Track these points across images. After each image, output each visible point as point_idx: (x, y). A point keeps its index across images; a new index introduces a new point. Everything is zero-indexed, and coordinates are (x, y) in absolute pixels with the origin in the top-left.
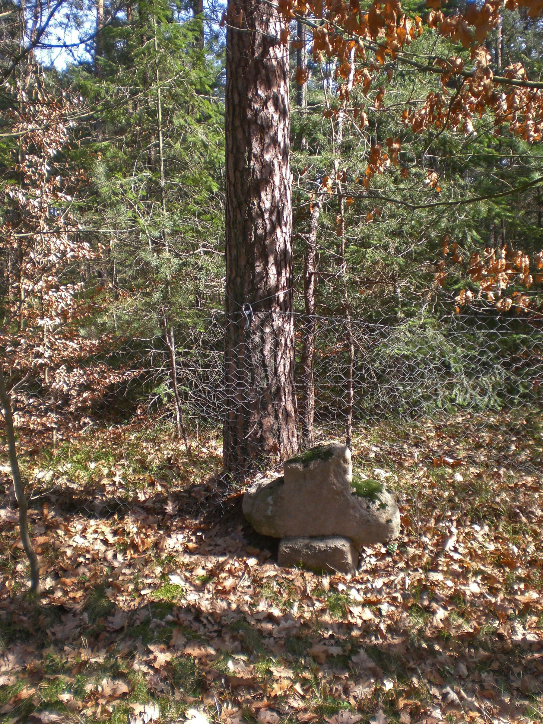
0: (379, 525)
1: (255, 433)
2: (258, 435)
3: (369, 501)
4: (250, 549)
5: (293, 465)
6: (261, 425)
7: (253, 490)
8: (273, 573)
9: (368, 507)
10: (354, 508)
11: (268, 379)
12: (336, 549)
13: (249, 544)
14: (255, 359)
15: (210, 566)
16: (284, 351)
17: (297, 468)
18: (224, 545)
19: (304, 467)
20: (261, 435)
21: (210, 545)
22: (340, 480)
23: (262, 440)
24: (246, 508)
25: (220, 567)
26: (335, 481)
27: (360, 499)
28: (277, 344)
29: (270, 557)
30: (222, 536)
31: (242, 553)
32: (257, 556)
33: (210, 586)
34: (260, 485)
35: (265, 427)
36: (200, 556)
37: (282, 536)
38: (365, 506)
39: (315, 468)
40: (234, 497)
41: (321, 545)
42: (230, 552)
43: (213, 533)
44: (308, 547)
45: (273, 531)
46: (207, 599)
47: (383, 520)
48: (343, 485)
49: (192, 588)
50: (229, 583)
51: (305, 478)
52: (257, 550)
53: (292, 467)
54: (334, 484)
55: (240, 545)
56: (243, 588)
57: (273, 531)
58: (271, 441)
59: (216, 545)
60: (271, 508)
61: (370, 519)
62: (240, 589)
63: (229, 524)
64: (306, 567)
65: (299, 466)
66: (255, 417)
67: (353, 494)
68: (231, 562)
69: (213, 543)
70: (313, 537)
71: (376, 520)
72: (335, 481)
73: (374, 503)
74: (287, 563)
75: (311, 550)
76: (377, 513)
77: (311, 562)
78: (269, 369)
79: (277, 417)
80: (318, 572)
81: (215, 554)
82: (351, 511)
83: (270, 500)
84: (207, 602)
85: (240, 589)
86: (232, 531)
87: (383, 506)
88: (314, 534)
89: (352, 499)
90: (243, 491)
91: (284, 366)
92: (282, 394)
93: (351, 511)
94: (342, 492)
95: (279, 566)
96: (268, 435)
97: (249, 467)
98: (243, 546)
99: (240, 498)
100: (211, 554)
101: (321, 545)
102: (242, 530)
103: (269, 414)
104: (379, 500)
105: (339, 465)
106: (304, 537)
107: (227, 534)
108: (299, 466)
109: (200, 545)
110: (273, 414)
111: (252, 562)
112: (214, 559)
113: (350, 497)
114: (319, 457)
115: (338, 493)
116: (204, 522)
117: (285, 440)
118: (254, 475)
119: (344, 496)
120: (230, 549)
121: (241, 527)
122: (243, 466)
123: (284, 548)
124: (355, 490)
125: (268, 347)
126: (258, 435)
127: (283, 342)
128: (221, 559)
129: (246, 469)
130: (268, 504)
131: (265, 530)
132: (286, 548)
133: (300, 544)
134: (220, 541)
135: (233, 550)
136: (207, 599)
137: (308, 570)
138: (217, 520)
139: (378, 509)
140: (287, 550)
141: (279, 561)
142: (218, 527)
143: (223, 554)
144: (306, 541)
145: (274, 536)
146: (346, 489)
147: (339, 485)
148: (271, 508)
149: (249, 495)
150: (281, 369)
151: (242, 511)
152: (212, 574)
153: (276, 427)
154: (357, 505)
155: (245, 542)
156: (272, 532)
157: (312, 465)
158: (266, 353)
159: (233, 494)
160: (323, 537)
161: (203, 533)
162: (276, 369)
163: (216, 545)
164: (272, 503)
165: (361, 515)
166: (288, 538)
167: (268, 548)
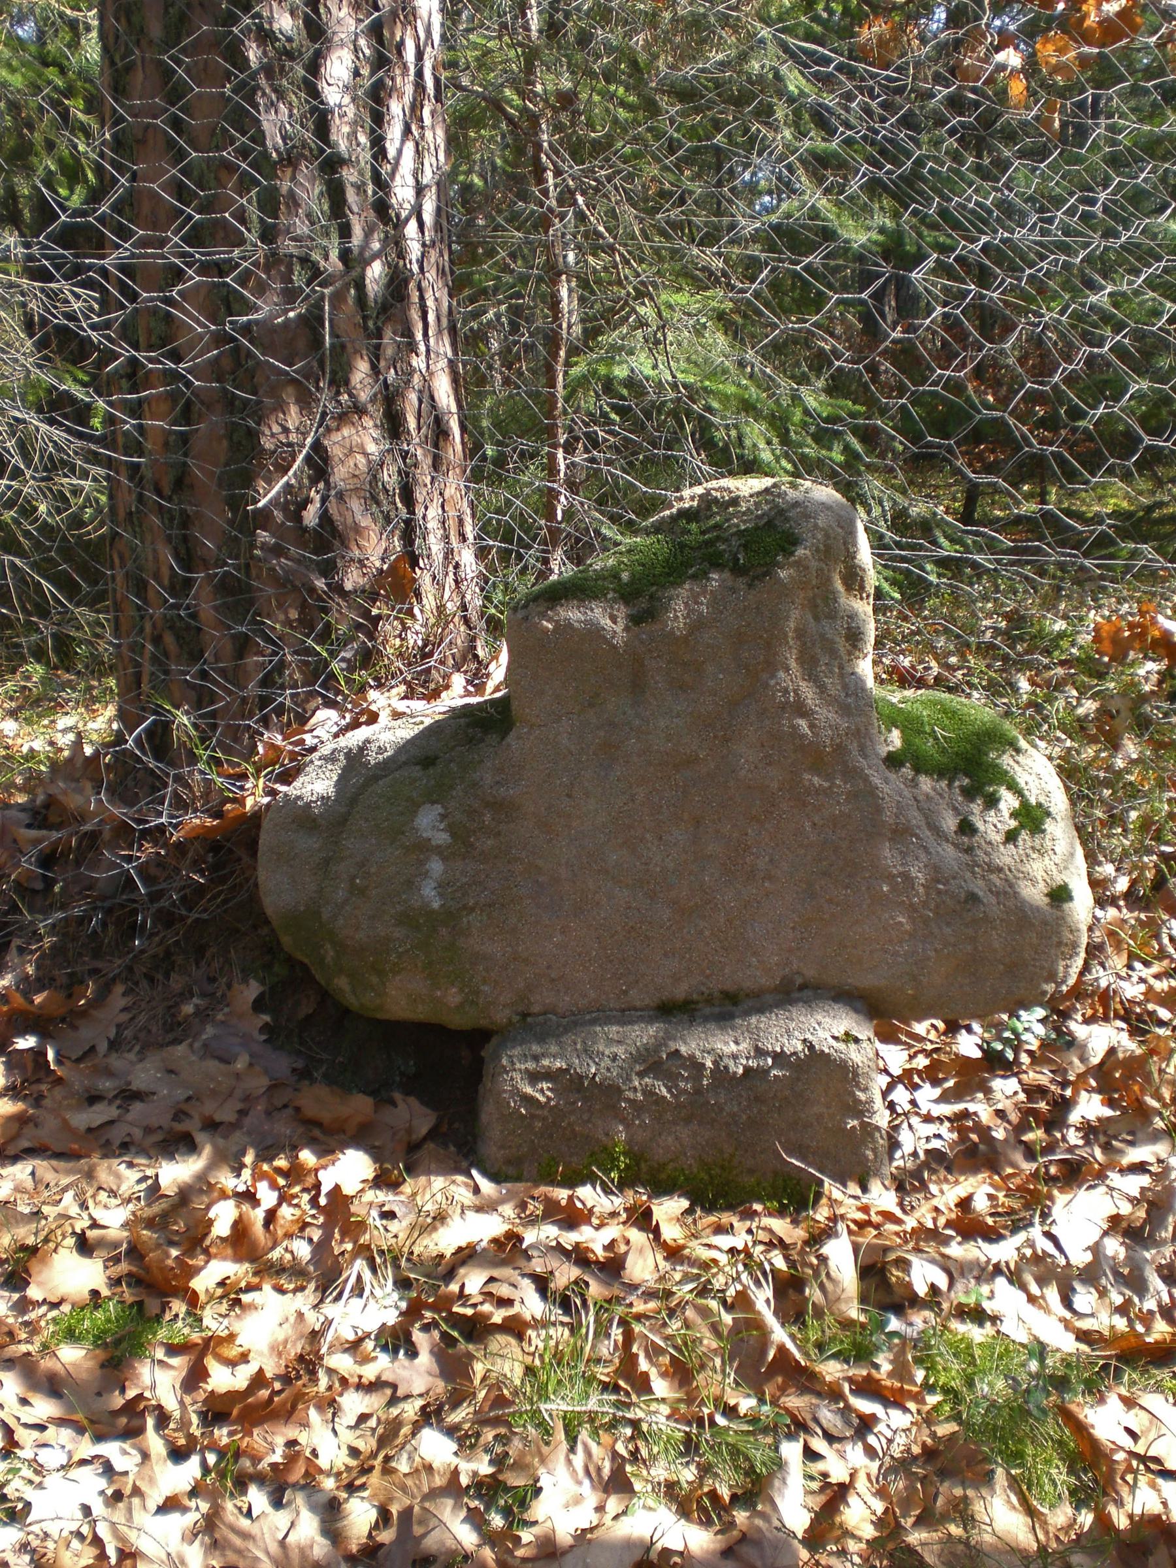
0: (1021, 917)
1: (295, 504)
2: (311, 516)
3: (970, 794)
4: (318, 1100)
5: (573, 614)
6: (320, 465)
7: (317, 785)
8: (484, 1229)
9: (967, 828)
10: (901, 834)
11: (345, 232)
12: (815, 1061)
13: (304, 1074)
14: (277, 123)
15: (114, 1219)
16: (416, 107)
17: (594, 632)
18: (168, 1093)
19: (636, 620)
20: (325, 517)
21: (93, 1099)
22: (832, 684)
23: (330, 539)
24: (278, 887)
25: (177, 1222)
26: (808, 693)
27: (926, 784)
28: (383, 56)
29: (432, 1135)
30: (147, 1045)
31: (286, 1127)
32: (360, 1138)
33: (159, 1380)
34: (355, 757)
35: (340, 474)
36: (42, 1166)
37: (501, 1016)
38: (950, 823)
39: (697, 625)
40: (202, 837)
41: (727, 1047)
42: (211, 1126)
43: (89, 1034)
44: (653, 1062)
45: (453, 996)
46: (170, 1505)
47: (1035, 893)
48: (845, 710)
49: (44, 1408)
50: (266, 1327)
51: (638, 685)
52: (360, 1105)
53: (564, 628)
54: (800, 709)
55: (260, 1083)
56: (354, 1347)
57: (453, 996)
58: (375, 548)
59: (129, 1096)
60: (436, 866)
61: (978, 887)
62: (342, 1363)
63: (177, 982)
64: (649, 1175)
65: (606, 619)
66: (290, 424)
67: (893, 761)
68: (228, 1181)
69: (107, 1085)
70: (676, 1011)
71: (1008, 892)
72: (808, 693)
73: (992, 802)
74: (541, 1159)
75: (671, 1079)
76: (1006, 856)
77: (676, 1143)
78: (349, 175)
79: (394, 426)
80: (715, 1194)
81: (125, 1148)
82: (888, 856)
83: (428, 823)
84: (179, 1522)
85: (342, 1363)
86: (203, 1015)
87: (1032, 818)
88: (680, 992)
89: (890, 786)
90: (255, 796)
91: (415, 168)
92: (415, 315)
93: (888, 856)
94: (840, 749)
95: (495, 1177)
96: (357, 511)
97: (267, 682)
98: (275, 1087)
99: (236, 841)
100: (108, 1152)
101: (727, 1047)
102: (259, 1005)
103: (360, 410)
104: (1013, 787)
105: (823, 605)
106: (626, 1015)
107: (176, 1030)
108: (606, 619)
109: (37, 1101)
110: (377, 411)
111: (350, 1169)
112: (128, 1177)
113: (877, 777)
114: (716, 562)
115: (816, 757)
116: (40, 983)
117: (436, 547)
118: (303, 719)
119: (852, 773)
120: (209, 1108)
121: (252, 990)
122: (236, 677)
123: (522, 1080)
124: (896, 738)
125: (339, 67)
126: (311, 516)
127: (410, 54)
128: (174, 1173)
129: (253, 689)
130: (424, 848)
131: (403, 997)
132: (534, 1077)
133: (611, 1051)
134: (145, 1075)
135: (226, 1114)
136: (170, 1505)
137: (662, 1189)
138: (117, 964)
139: (1011, 837)
140: (542, 1092)
141: (491, 1150)
142: (118, 999)
143: (177, 1143)
144: (644, 1034)
145: (457, 1021)
146: (862, 737)
147: (826, 714)
148: (436, 866)
149: (301, 816)
150: (402, 193)
151: (254, 899)
152: (150, 1282)
153: (389, 477)
154: (915, 818)
155: (283, 1064)
156: (449, 1004)
157: (680, 609)
158: (333, 96)
159: (195, 820)
160: (730, 1006)
161: (45, 1035)
162: (382, 185)
163: (129, 1096)
164: (442, 838)
165: (937, 874)
166: (533, 1025)
167: (429, 1089)
